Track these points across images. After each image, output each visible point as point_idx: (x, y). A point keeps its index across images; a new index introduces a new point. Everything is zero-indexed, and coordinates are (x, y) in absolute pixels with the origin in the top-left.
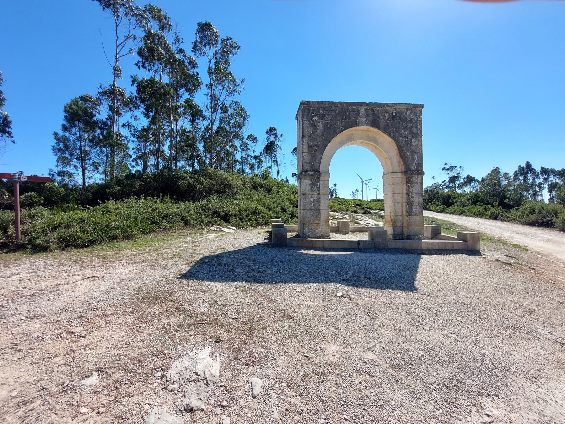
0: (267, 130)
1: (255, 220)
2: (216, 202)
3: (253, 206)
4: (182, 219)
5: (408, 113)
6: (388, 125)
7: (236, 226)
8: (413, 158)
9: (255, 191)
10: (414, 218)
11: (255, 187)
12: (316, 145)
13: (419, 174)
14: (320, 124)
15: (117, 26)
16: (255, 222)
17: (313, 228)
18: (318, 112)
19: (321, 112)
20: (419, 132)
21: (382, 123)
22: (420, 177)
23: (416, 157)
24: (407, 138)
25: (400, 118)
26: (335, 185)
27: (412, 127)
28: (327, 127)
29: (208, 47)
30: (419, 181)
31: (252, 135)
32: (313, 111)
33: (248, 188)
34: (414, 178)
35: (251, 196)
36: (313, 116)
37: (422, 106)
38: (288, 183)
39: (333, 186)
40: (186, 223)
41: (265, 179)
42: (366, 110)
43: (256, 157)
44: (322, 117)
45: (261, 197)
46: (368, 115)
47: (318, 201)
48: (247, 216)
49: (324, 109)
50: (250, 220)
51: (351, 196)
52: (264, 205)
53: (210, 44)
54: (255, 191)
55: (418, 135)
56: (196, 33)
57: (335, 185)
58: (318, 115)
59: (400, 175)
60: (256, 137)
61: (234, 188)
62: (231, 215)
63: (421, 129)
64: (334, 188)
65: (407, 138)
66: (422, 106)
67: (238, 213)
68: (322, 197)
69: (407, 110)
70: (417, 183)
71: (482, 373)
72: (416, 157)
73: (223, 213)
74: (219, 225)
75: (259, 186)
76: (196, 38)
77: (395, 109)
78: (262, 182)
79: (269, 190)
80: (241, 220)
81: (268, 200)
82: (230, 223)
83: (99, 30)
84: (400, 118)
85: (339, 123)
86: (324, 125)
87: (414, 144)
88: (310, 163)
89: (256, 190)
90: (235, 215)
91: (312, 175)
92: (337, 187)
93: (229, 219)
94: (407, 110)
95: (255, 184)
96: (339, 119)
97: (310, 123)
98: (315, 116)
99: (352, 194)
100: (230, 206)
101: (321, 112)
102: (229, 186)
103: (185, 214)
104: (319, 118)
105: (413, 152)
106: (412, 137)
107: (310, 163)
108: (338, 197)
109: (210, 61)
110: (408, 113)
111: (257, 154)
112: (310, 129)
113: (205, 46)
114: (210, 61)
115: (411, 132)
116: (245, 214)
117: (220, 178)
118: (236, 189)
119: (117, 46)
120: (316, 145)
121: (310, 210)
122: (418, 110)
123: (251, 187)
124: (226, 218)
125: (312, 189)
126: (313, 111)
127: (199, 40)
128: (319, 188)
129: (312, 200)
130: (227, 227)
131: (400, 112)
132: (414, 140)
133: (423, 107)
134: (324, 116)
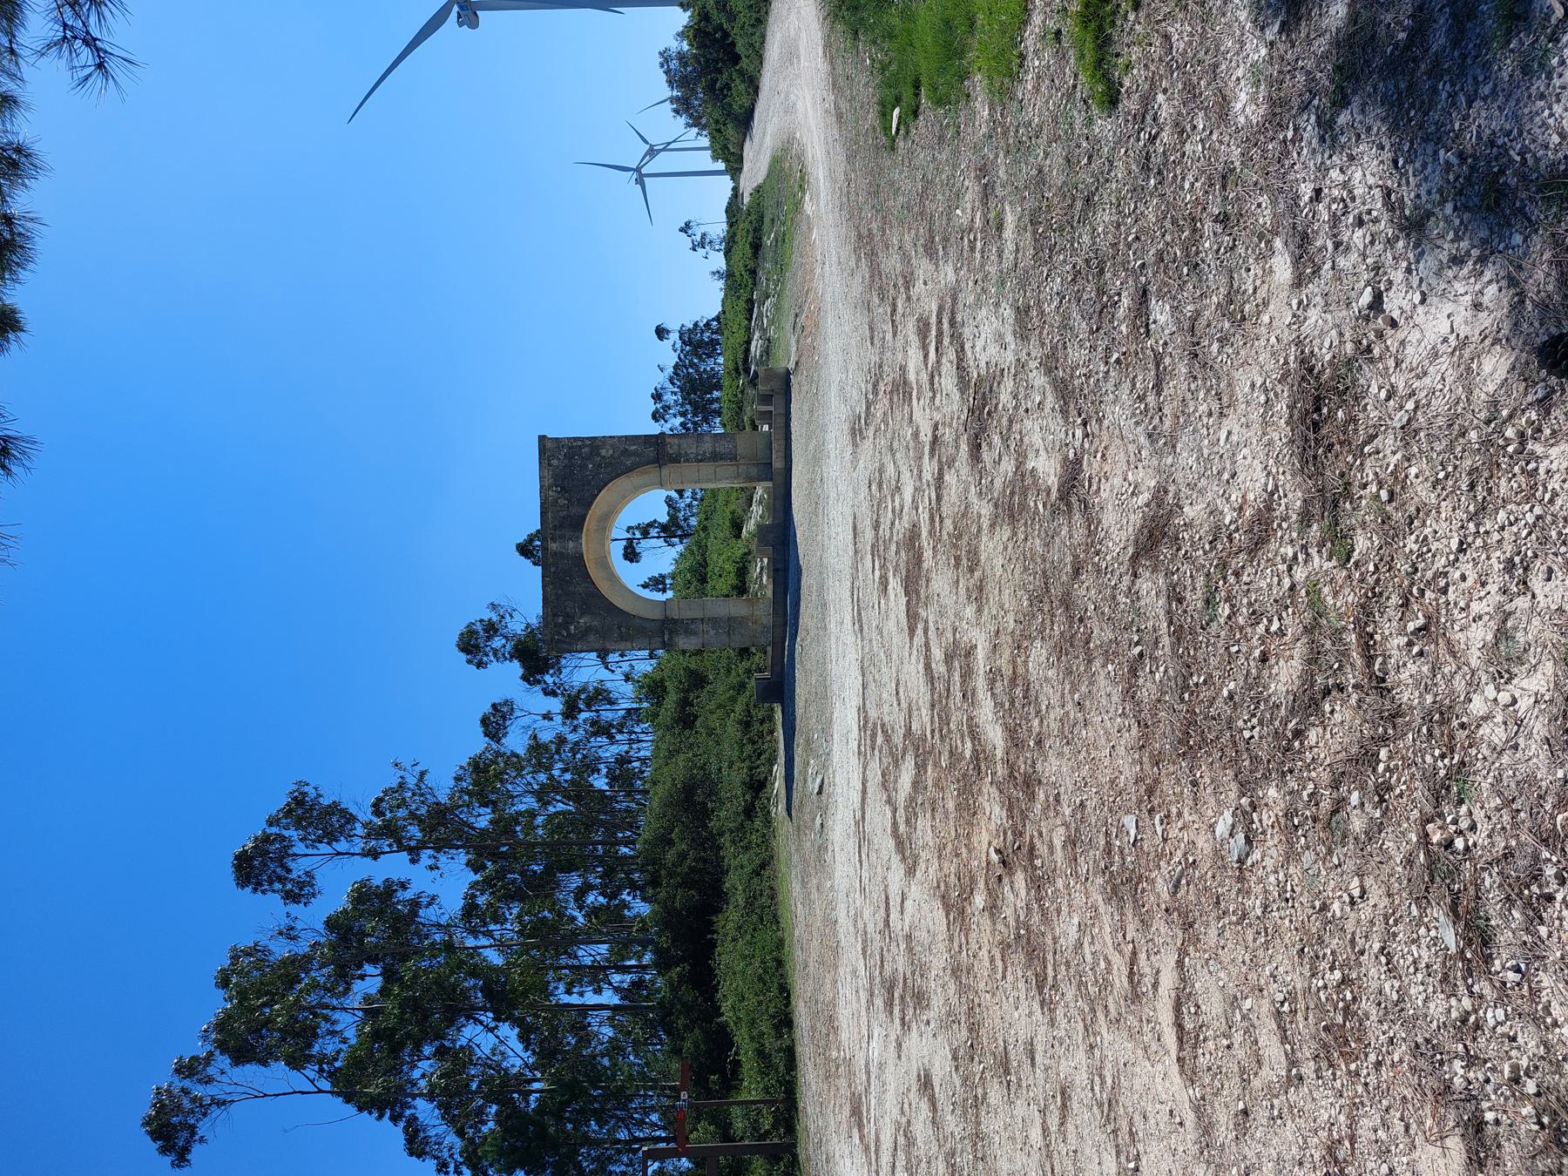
0: (469, 662)
1: (761, 724)
2: (725, 816)
3: (732, 730)
4: (758, 875)
5: (555, 462)
6: (578, 500)
7: (772, 765)
8: (635, 453)
9: (699, 720)
10: (740, 451)
11: (686, 720)
12: (619, 627)
13: (664, 444)
14: (582, 621)
15: (266, 1095)
16: (766, 726)
17: (760, 629)
18: (560, 625)
19: (560, 620)
20: (588, 443)
21: (575, 510)
22: (668, 440)
23: (633, 448)
24: (600, 465)
25: (564, 478)
26: (661, 333)
27: (580, 455)
28: (585, 610)
29: (292, 865)
30: (676, 441)
31: (485, 721)
32: (559, 633)
33: (692, 740)
34: (671, 452)
35: (710, 732)
36: (569, 634)
37: (542, 439)
38: (663, 577)
39: (667, 344)
40: (763, 866)
41: (665, 690)
42: (554, 540)
43: (570, 711)
44: (569, 618)
45: (712, 706)
46: (562, 537)
47: (714, 621)
48: (754, 743)
49: (555, 615)
50: (761, 736)
51: (712, 254)
52: (733, 700)
53: (284, 855)
54: (698, 723)
55: (595, 444)
56: (263, 892)
57: (661, 333)
58: (565, 625)
59: (665, 471)
60: (494, 706)
61: (693, 777)
62: (751, 776)
63: (582, 439)
64: (674, 337)
65: (600, 465)
66: (542, 439)
67: (747, 763)
68: (709, 614)
69: (550, 465)
70: (679, 446)
71: (743, 686)
72: (633, 448)
73: (748, 797)
74: (769, 800)
75: (683, 708)
76: (274, 891)
77: (550, 487)
78: (671, 700)
79: (697, 680)
80: (760, 755)
81: (720, 688)
82: (766, 778)
83: (285, 1131)
84: (564, 478)
85: (579, 589)
86: (583, 614)
87: (611, 452)
88: (650, 638)
89: (696, 717)
90: (751, 769)
91: (671, 634)
92: (673, 325)
93: (759, 781)
94: (550, 465)
95: (677, 721)
96: (572, 588)
97: (579, 639)
98: (568, 630)
99: (701, 251)
100: (733, 780)
101: (560, 620)
102: (689, 790)
103: (748, 870)
104: (571, 624)
105: (625, 452)
106: (598, 454)
107: (650, 638)
108: (717, 319)
109: (339, 854)
110: (555, 462)
111: (556, 705)
112: (592, 638)
113: (289, 871)
114: (339, 854)
115: (589, 458)
116: (750, 747)
117: (668, 803)
118: (695, 772)
119: (320, 1091)
120: (619, 627)
121: (729, 635)
122: (549, 445)
123: (687, 732)
124: (758, 786)
125: (696, 634)
126: (559, 633)
127: (277, 886)
128: (693, 620)
129: (712, 632)
130: (773, 784)
131: (555, 477)
132: (603, 452)
133: (544, 437)
134: (568, 615)
